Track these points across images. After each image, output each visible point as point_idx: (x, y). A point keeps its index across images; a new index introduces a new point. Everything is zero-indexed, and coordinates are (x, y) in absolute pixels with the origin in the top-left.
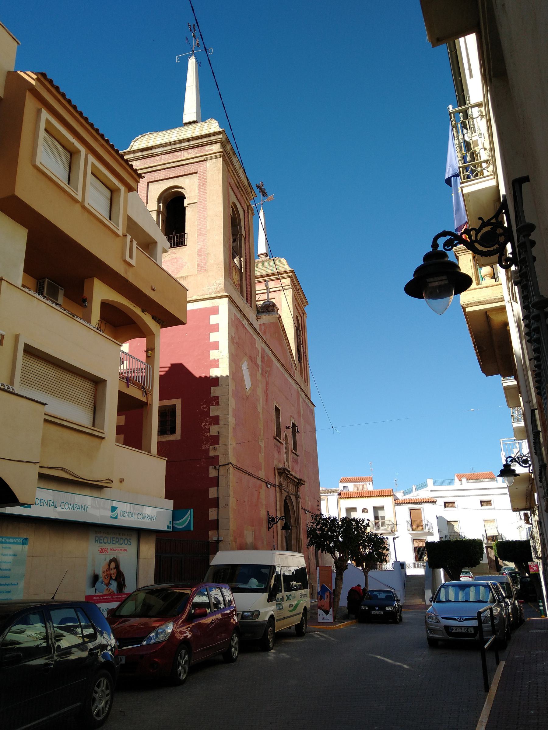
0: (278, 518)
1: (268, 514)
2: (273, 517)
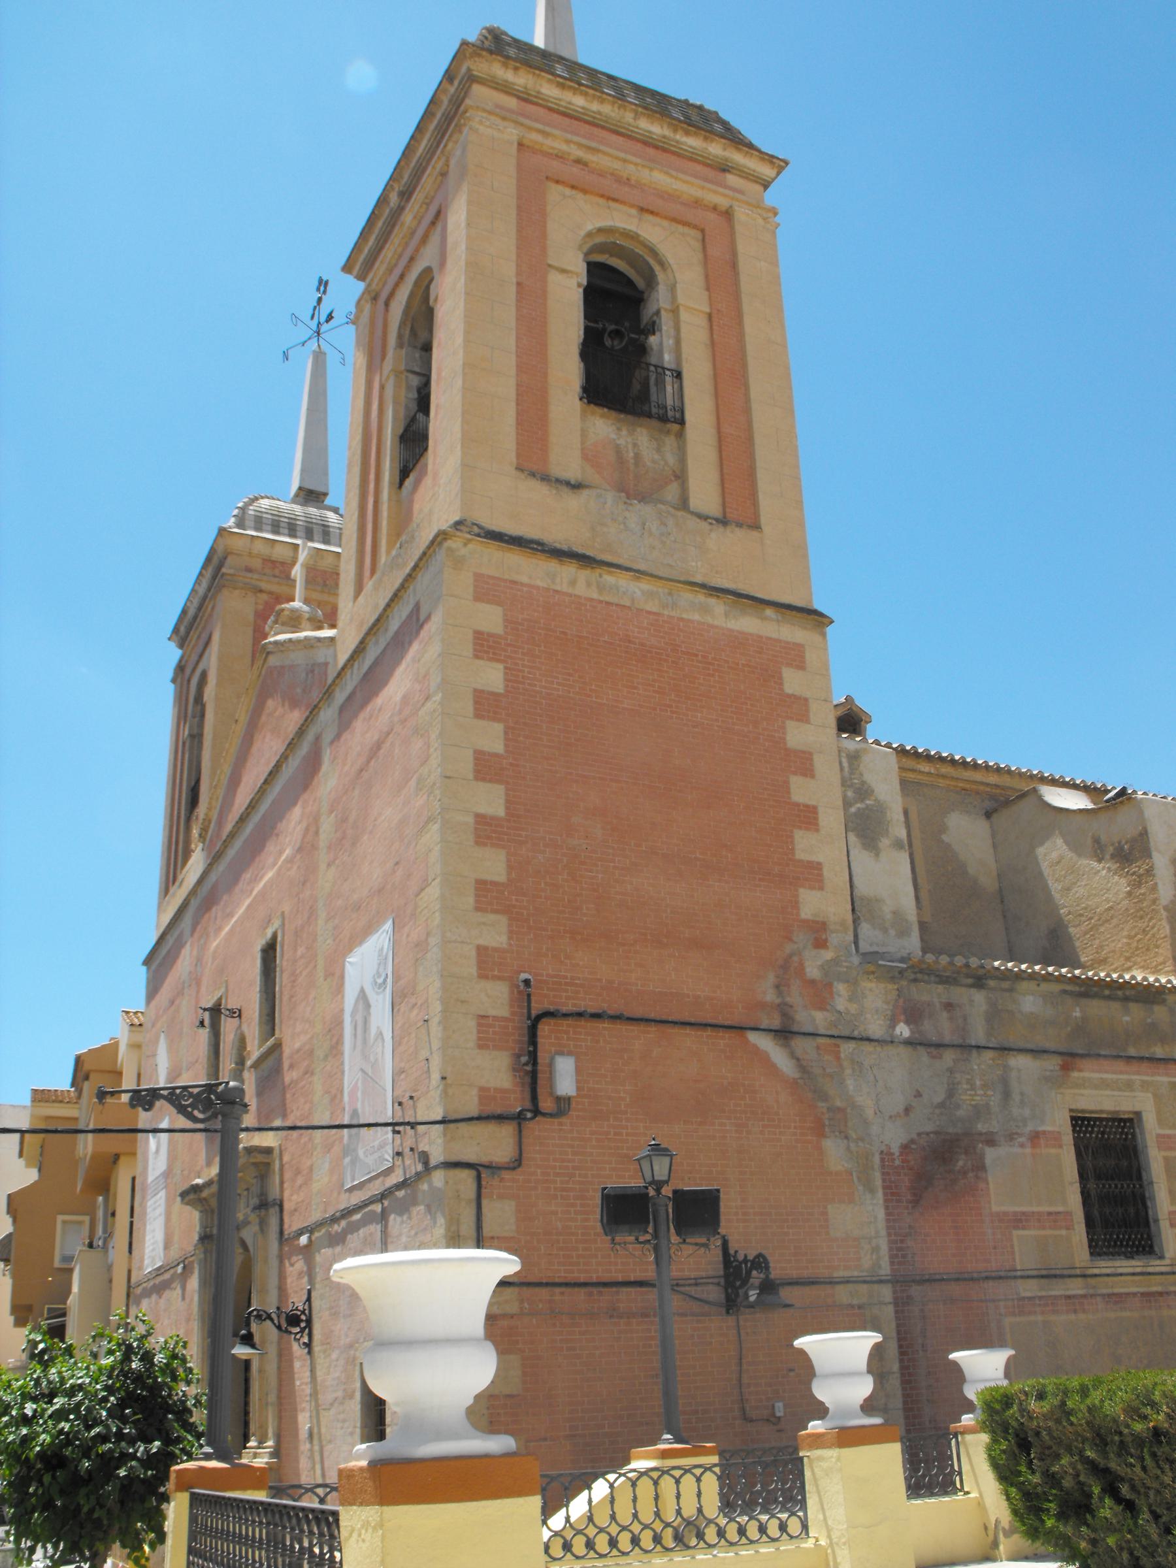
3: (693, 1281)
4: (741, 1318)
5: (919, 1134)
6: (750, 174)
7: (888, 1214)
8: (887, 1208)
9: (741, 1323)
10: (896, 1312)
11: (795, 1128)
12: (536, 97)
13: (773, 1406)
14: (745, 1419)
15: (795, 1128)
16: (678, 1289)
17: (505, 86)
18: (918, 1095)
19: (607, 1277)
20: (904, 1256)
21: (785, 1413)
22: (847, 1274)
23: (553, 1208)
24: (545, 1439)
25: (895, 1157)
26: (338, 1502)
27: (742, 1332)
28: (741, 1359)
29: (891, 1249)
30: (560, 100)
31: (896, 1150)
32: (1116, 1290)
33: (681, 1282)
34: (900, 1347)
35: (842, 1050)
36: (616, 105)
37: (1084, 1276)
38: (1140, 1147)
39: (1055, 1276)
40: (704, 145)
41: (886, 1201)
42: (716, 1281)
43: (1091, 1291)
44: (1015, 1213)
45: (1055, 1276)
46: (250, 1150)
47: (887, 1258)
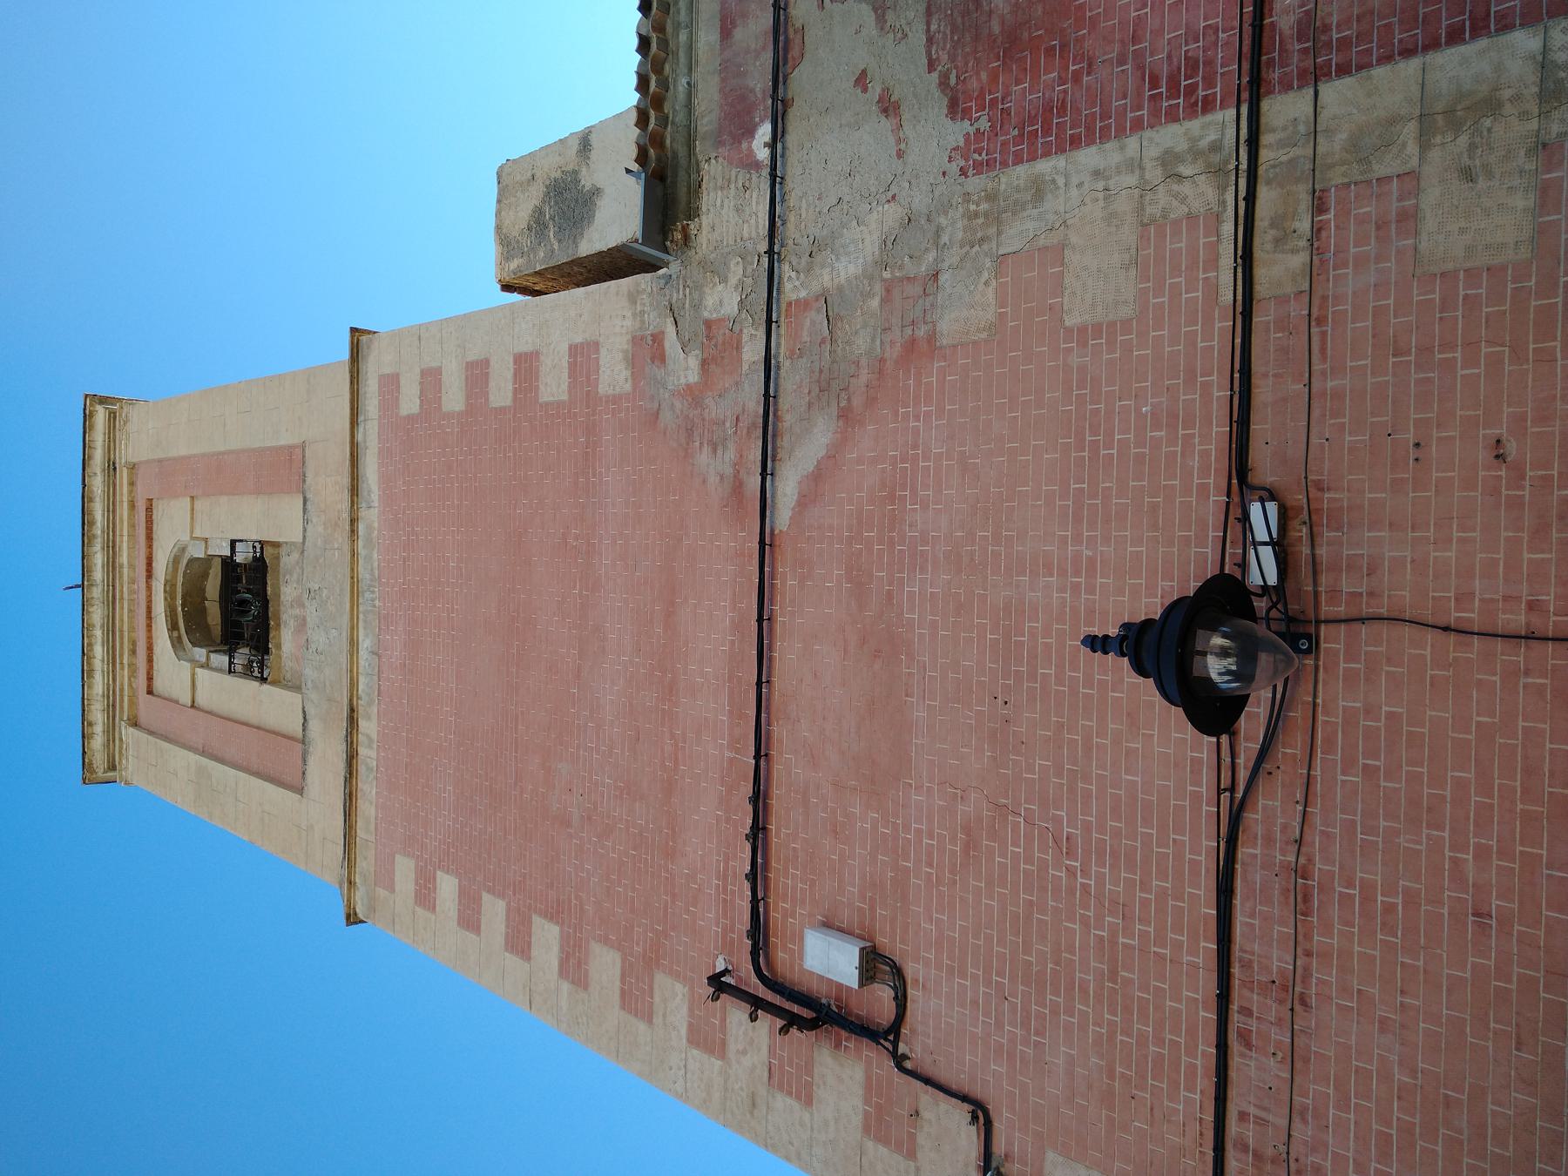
4: (1326, 610)
5: (931, 66)
6: (109, 438)
8: (1075, 142)
9: (1341, 610)
11: (917, 418)
12: (108, 697)
17: (108, 732)
19: (1207, 983)
23: (1061, 1061)
25: (972, 130)
26: (1195, 108)
27: (1366, 611)
29: (1172, 116)
30: (103, 672)
33: (1225, 782)
35: (794, 297)
36: (91, 610)
40: (98, 499)
47: (1194, 125)
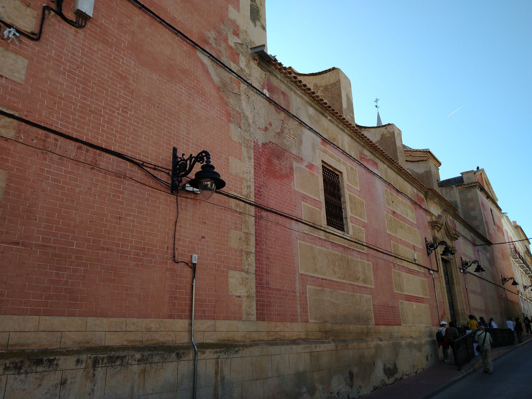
0: (471, 262)
1: (426, 241)
2: (466, 262)
3: (153, 167)
7: (255, 172)
8: (255, 169)
10: (256, 222)
11: (217, 110)
13: (191, 256)
14: (174, 260)
15: (217, 110)
16: (142, 166)
18: (270, 124)
20: (261, 195)
21: (198, 261)
22: (236, 194)
24: (17, 244)
28: (176, 222)
31: (260, 143)
32: (334, 242)
33: (145, 164)
34: (256, 240)
37: (325, 231)
38: (341, 187)
39: (316, 228)
41: (255, 165)
42: (167, 171)
43: (327, 239)
44: (303, 194)
45: (316, 228)
46: (56, 214)
47: (253, 193)
